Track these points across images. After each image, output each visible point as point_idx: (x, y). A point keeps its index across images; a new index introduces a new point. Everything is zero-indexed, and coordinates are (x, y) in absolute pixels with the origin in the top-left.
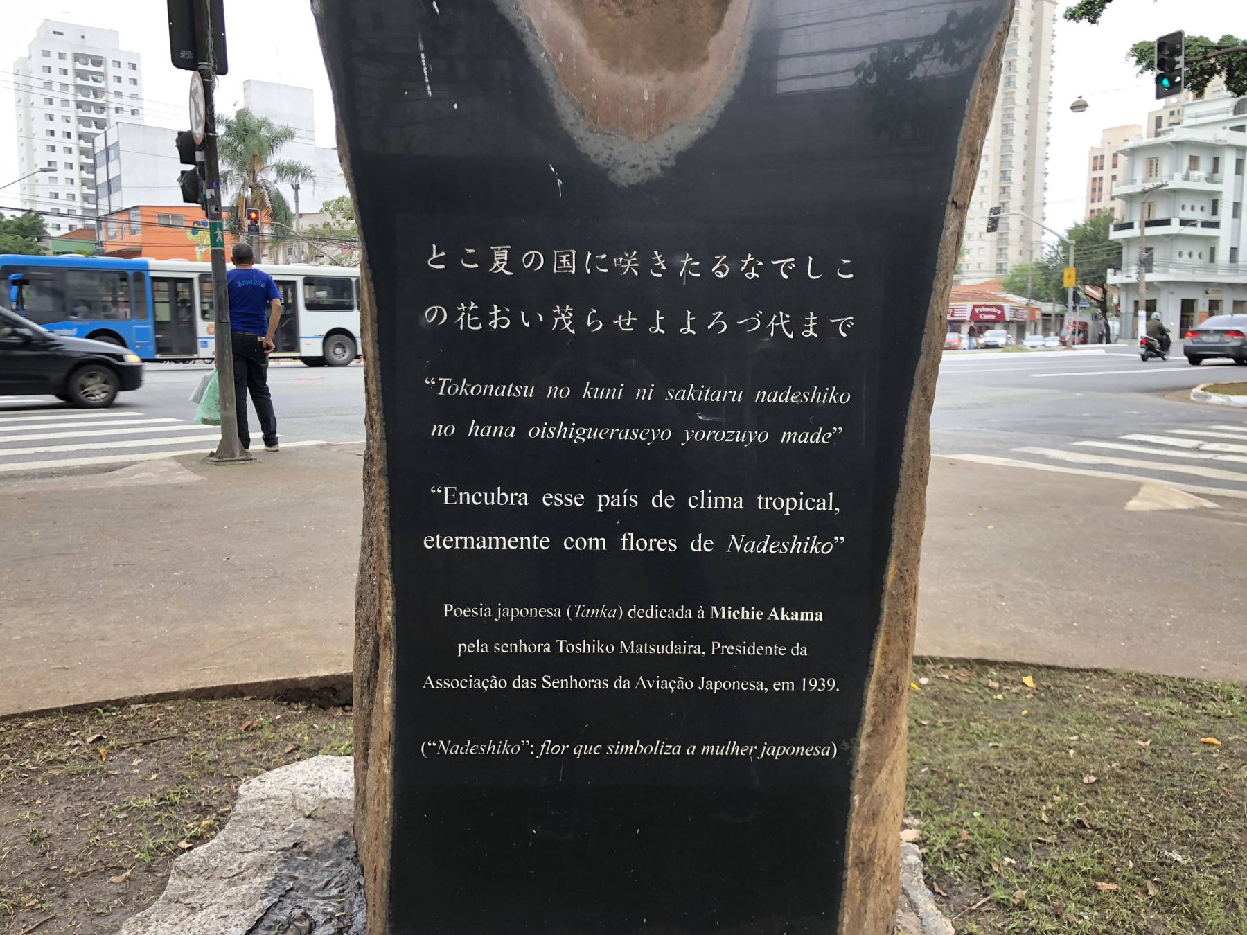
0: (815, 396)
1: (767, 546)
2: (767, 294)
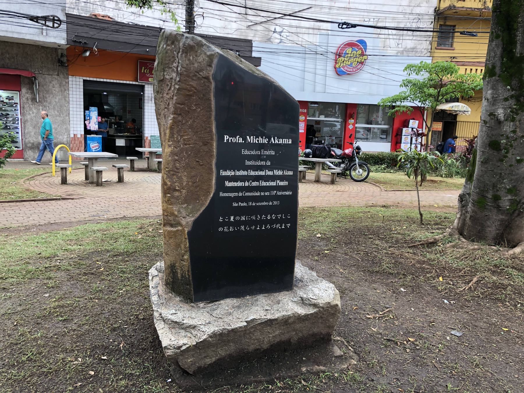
2: (277, 221)
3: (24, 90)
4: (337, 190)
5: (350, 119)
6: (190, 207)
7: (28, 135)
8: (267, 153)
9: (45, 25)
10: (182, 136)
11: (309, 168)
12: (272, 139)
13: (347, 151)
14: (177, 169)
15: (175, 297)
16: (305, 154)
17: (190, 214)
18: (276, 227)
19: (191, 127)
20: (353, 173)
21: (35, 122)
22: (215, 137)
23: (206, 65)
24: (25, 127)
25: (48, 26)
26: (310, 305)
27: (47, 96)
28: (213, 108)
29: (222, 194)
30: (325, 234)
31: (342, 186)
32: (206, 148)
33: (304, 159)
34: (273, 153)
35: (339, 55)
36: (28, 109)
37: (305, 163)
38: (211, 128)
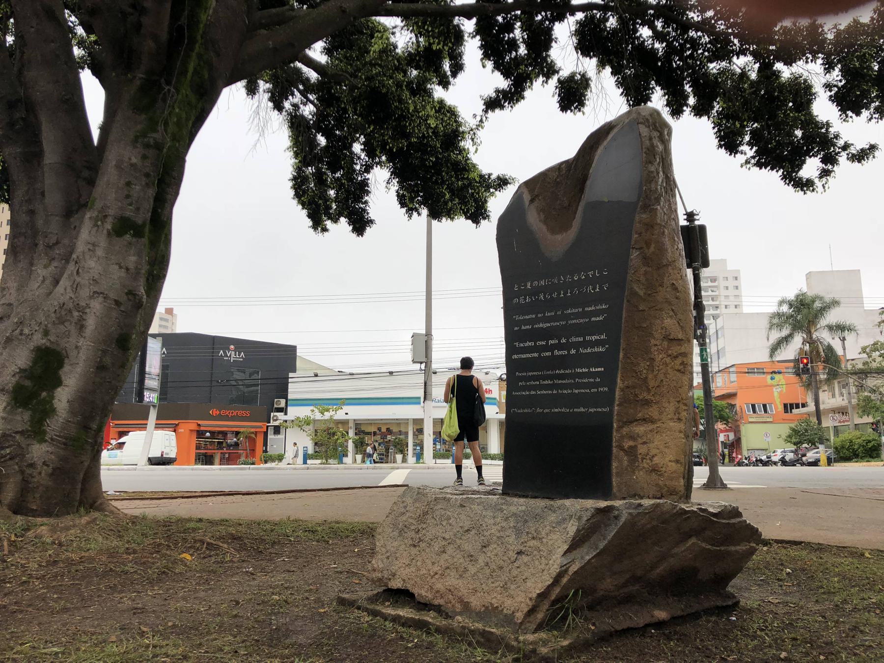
0: (599, 307)
1: (589, 350)
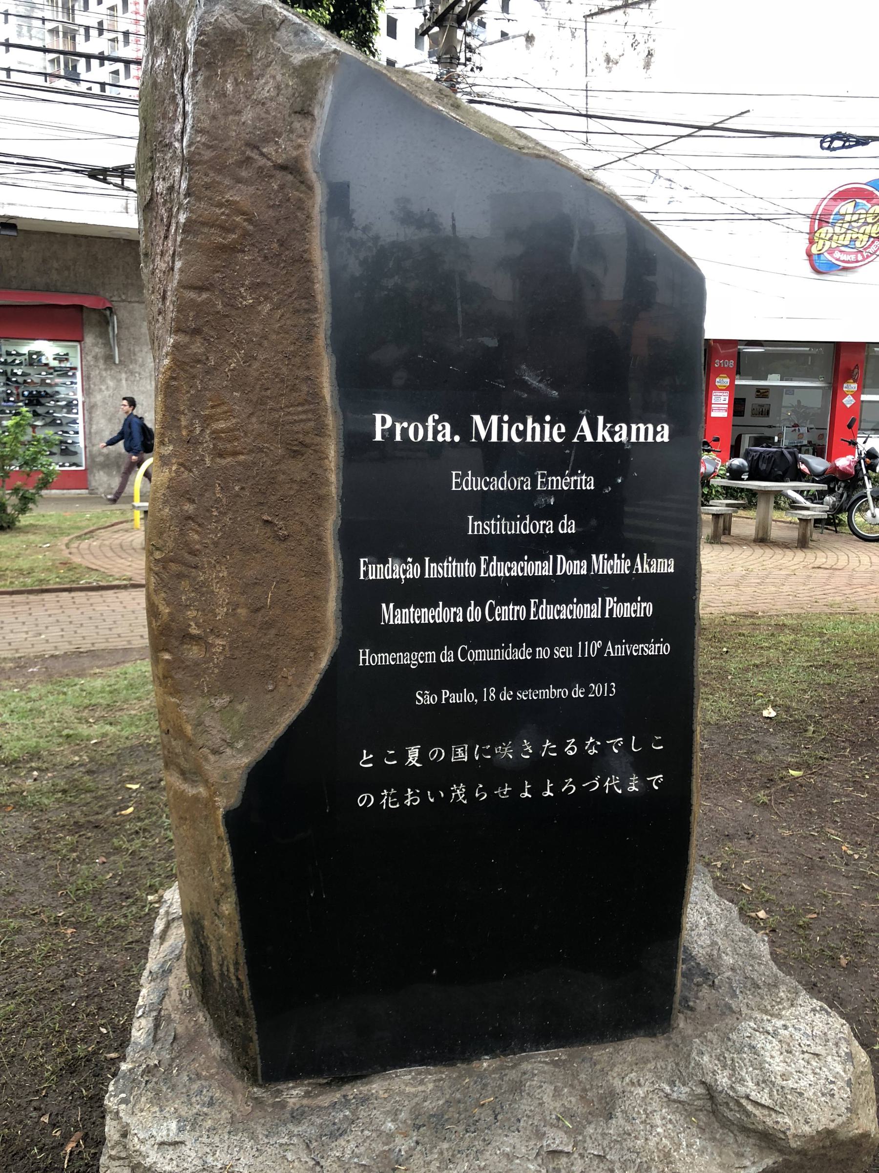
3: (89, 339)
4: (817, 564)
5: (846, 380)
6: (242, 708)
7: (98, 438)
8: (563, 483)
9: (122, 187)
10: (207, 421)
11: (738, 506)
12: (584, 423)
13: (843, 462)
14: (193, 553)
15: (210, 1035)
16: (730, 470)
17: (236, 737)
18: (602, 788)
19: (239, 381)
20: (857, 519)
21: (112, 409)
22: (332, 421)
23: (286, 112)
24: (91, 419)
25: (128, 189)
26: (745, 1130)
27: (137, 349)
28: (320, 298)
29: (366, 658)
30: (788, 709)
31: (829, 554)
32: (296, 469)
33: (726, 482)
34: (586, 483)
35: (821, 219)
36: (97, 380)
37: (729, 492)
38: (312, 381)
